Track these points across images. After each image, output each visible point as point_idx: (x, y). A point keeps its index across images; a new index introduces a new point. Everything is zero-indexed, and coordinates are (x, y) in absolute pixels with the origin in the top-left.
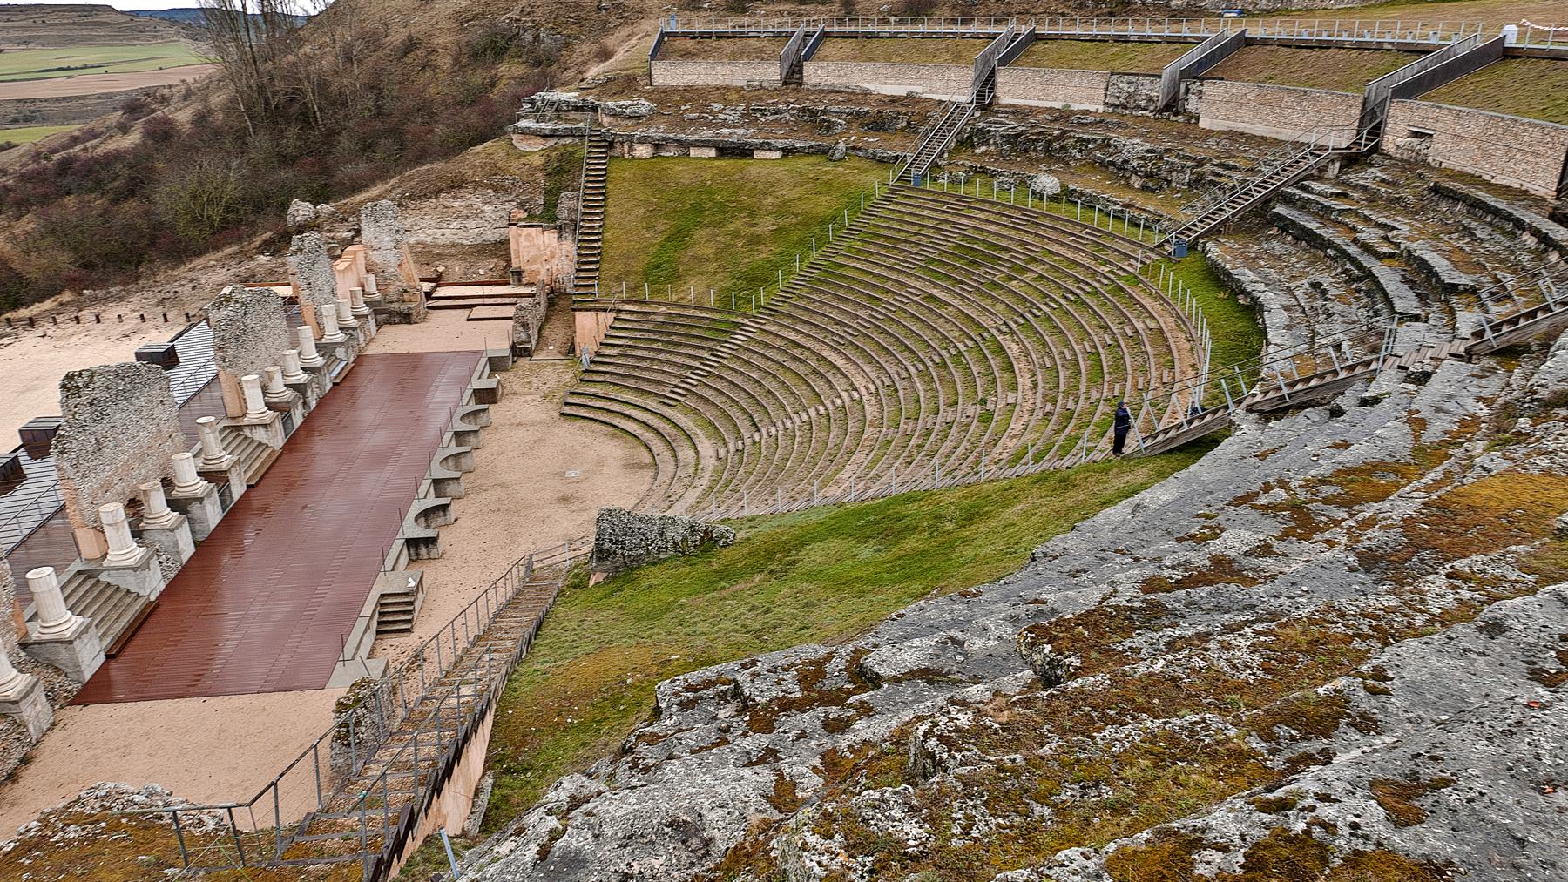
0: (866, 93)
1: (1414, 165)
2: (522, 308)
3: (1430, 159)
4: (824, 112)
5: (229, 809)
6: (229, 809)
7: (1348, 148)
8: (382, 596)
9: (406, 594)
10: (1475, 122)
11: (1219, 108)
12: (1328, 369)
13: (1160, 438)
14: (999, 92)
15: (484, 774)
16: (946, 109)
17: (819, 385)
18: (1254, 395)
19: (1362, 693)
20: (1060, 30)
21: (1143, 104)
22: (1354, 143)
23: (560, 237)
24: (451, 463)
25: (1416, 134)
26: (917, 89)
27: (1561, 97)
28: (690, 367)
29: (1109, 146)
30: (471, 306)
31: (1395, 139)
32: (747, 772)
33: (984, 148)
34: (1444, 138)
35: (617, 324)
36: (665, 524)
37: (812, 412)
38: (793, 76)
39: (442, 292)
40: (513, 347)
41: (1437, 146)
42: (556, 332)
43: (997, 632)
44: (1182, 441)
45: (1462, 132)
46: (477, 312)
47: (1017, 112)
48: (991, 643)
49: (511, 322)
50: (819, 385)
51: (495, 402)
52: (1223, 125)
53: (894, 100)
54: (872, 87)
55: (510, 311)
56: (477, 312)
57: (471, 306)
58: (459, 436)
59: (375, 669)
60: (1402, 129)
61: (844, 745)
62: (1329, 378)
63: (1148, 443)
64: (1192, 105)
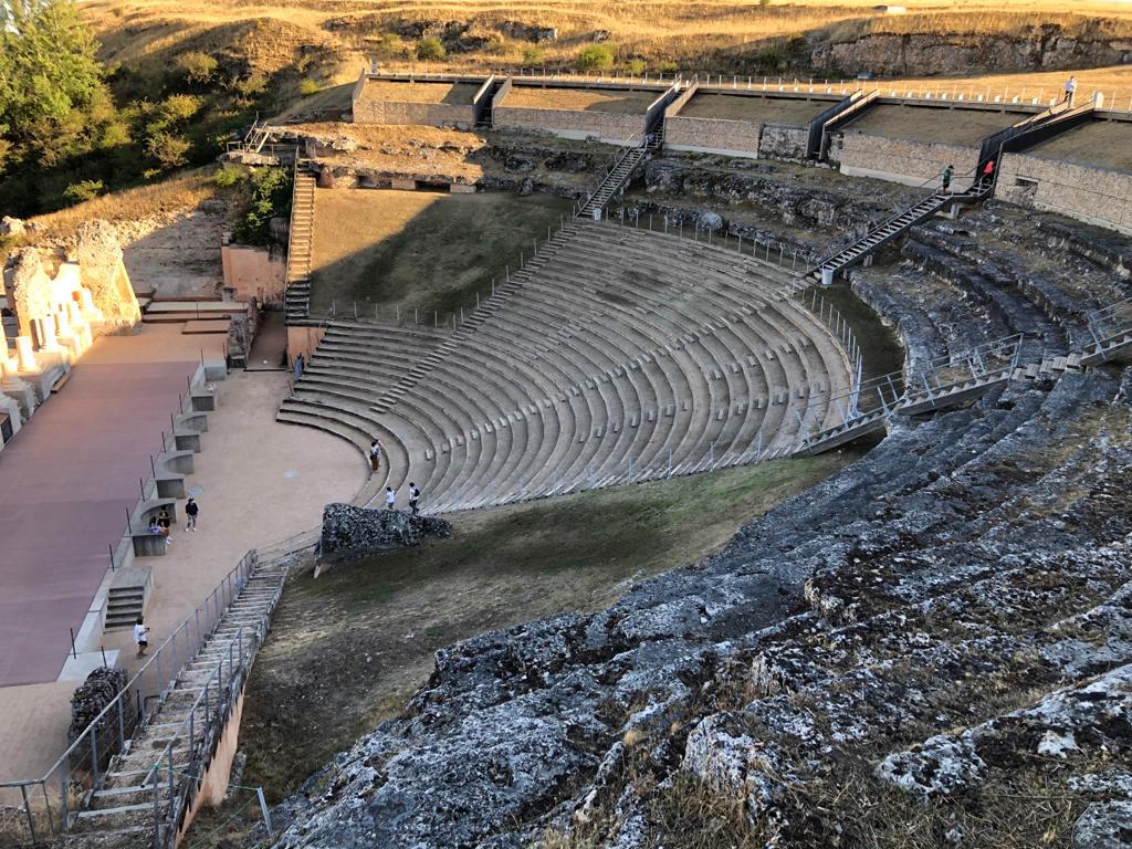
0: (551, 135)
1: (1027, 211)
2: (236, 323)
3: (1035, 204)
4: (514, 152)
5: (23, 786)
6: (23, 786)
7: (966, 193)
8: (111, 591)
9: (135, 589)
10: (1073, 174)
11: (857, 158)
12: (966, 379)
13: (824, 438)
14: (668, 138)
15: (238, 751)
16: (622, 151)
17: (514, 393)
18: (903, 401)
19: (1118, 617)
20: (720, 86)
21: (792, 152)
22: (971, 189)
23: (270, 258)
24: (173, 465)
25: (1021, 183)
26: (594, 134)
27: (27, 2)
28: (397, 378)
29: (763, 187)
30: (185, 321)
31: (1005, 187)
32: (539, 722)
33: (654, 188)
34: (1047, 186)
35: (328, 339)
36: (386, 517)
37: (511, 419)
38: (818, 148)
39: (154, 307)
40: (228, 360)
41: (1041, 193)
42: (270, 341)
43: (732, 599)
44: (822, 449)
45: (1063, 182)
46: (191, 326)
47: (682, 156)
48: (727, 607)
49: (227, 335)
50: (514, 393)
51: (212, 409)
52: (862, 172)
53: (574, 143)
54: (555, 131)
55: (225, 325)
56: (191, 326)
57: (185, 321)
58: (181, 442)
59: (112, 659)
60: (1012, 179)
61: (618, 695)
62: (967, 387)
63: (813, 444)
64: (834, 154)
